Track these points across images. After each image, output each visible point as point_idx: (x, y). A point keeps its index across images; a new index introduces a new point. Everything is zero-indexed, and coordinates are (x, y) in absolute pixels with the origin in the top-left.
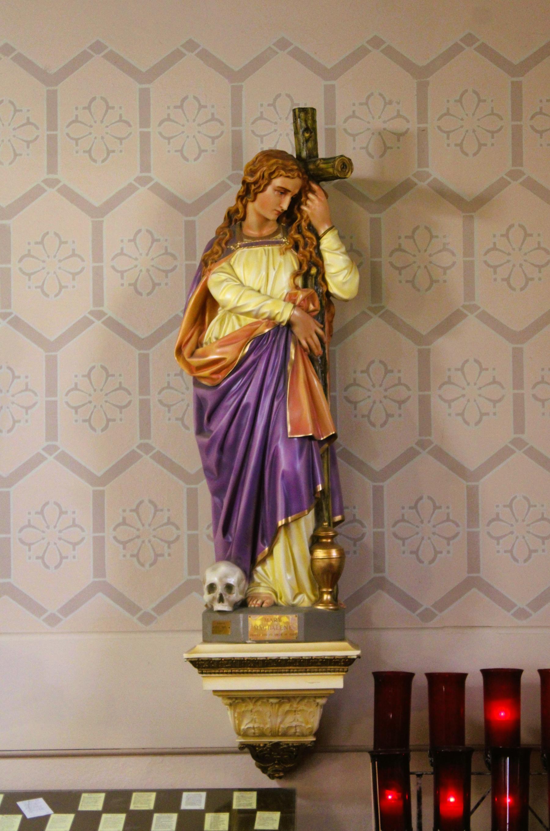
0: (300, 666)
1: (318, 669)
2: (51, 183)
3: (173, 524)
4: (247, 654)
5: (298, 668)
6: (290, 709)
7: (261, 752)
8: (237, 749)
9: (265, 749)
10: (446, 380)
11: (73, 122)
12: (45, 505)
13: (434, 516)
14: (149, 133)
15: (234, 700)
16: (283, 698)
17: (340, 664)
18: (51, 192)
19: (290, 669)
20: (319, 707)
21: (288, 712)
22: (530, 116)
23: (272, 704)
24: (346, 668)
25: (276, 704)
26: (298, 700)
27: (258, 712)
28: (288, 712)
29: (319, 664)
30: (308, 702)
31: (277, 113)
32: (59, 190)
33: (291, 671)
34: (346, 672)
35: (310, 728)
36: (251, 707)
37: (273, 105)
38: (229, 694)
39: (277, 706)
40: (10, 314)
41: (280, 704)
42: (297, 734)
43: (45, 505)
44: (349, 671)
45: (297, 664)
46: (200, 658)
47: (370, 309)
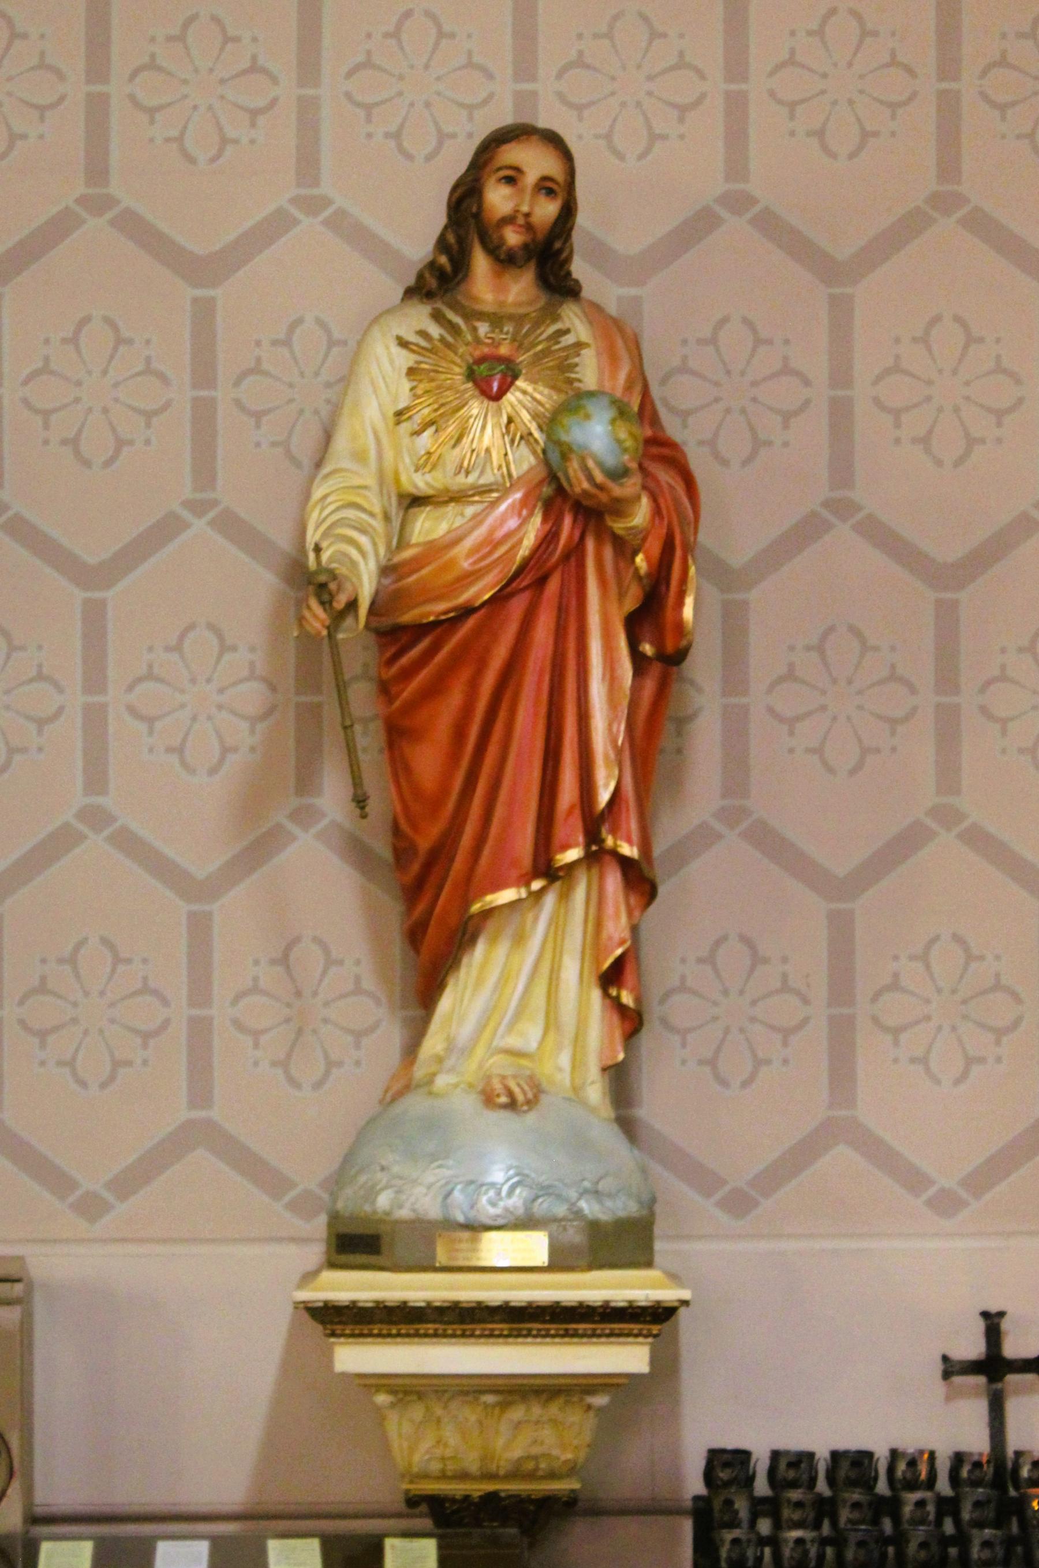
0: (552, 1321)
1: (344, 1330)
2: (99, 204)
3: (155, 993)
4: (618, 1292)
5: (547, 1326)
6: (526, 1418)
7: (454, 1512)
8: (402, 1506)
9: (464, 1505)
10: (996, 672)
11: (783, 65)
12: (718, 943)
13: (326, 981)
14: (534, 94)
15: (400, 1396)
16: (510, 1392)
17: (642, 1319)
18: (308, 224)
19: (493, 1330)
20: (591, 1414)
21: (518, 1425)
22: (345, 69)
23: (486, 1406)
24: (655, 1329)
25: (494, 1406)
26: (544, 1396)
27: (554, 1422)
28: (518, 1425)
29: (596, 1319)
30: (567, 1402)
31: (617, 51)
32: (754, 221)
33: (497, 1333)
34: (655, 1336)
35: (569, 1460)
36: (536, 1410)
37: (819, 33)
38: (392, 1381)
39: (497, 1411)
40: (215, 503)
41: (504, 1406)
42: (540, 1473)
43: (718, 943)
44: (661, 1337)
45: (548, 1318)
46: (331, 1301)
47: (188, 504)
